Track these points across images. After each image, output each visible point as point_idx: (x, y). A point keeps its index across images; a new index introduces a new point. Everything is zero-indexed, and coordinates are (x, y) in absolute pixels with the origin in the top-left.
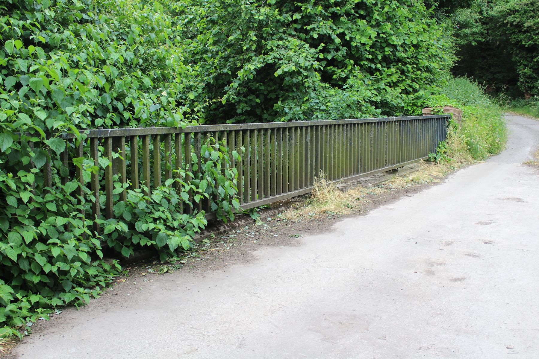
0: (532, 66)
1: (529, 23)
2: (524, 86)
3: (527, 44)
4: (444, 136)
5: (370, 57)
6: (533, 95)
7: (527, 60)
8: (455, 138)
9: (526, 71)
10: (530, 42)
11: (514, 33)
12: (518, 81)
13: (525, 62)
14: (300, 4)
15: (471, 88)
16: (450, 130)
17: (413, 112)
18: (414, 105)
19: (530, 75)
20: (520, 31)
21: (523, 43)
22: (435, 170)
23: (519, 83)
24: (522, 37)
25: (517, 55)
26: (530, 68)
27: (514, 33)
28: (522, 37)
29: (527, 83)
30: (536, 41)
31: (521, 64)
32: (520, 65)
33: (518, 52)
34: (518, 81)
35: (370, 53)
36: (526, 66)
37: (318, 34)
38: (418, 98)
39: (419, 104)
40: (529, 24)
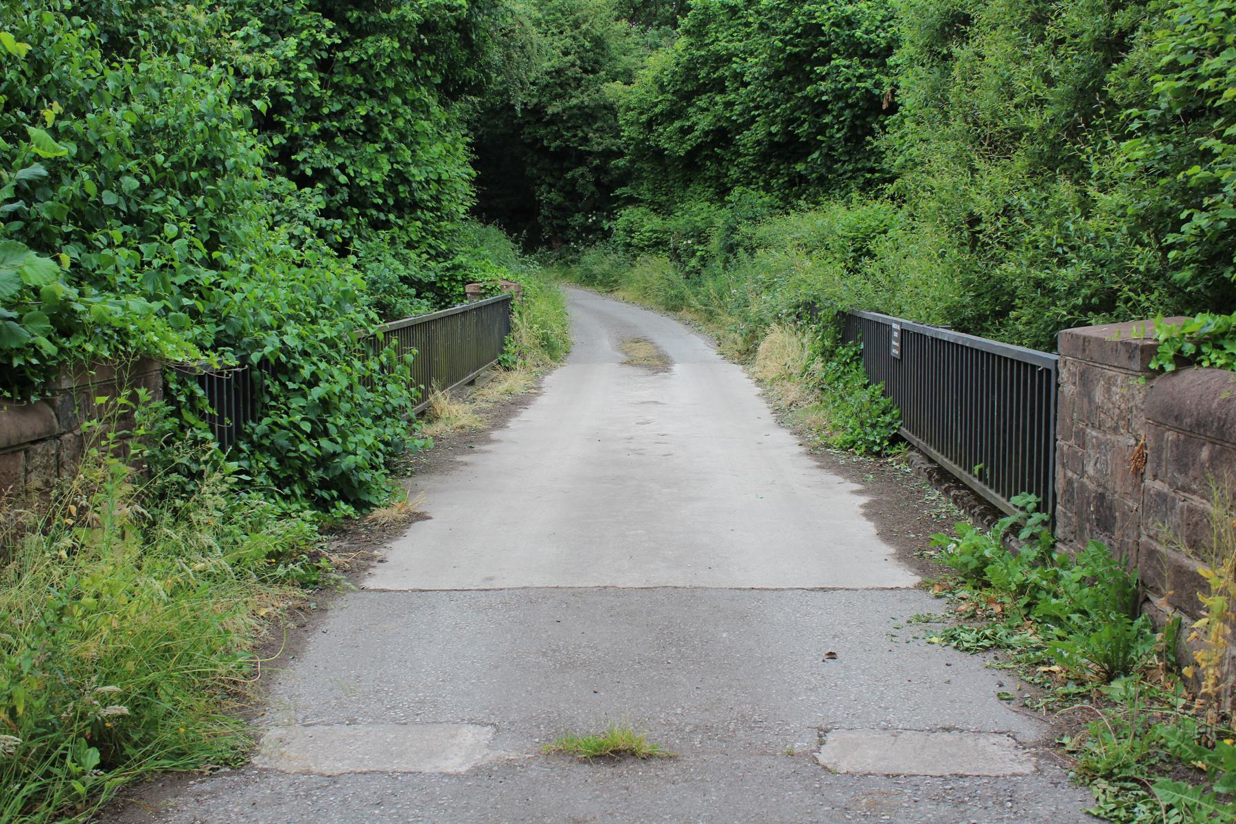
0: (563, 187)
1: (554, 108)
2: (551, 224)
3: (553, 145)
4: (508, 329)
5: (380, 202)
6: (567, 242)
7: (552, 176)
8: (524, 332)
9: (552, 195)
10: (558, 142)
11: (528, 122)
12: (539, 214)
13: (549, 180)
14: (283, 119)
15: (495, 234)
16: (515, 319)
17: (451, 290)
18: (452, 279)
19: (559, 204)
20: (539, 120)
21: (545, 143)
22: (516, 381)
23: (540, 219)
24: (543, 132)
25: (534, 165)
26: (559, 191)
27: (528, 122)
28: (543, 132)
29: (556, 218)
30: (568, 140)
31: (543, 182)
32: (540, 185)
33: (536, 158)
34: (539, 214)
35: (381, 195)
36: (551, 186)
37: (312, 168)
38: (455, 267)
39: (459, 278)
40: (555, 110)
